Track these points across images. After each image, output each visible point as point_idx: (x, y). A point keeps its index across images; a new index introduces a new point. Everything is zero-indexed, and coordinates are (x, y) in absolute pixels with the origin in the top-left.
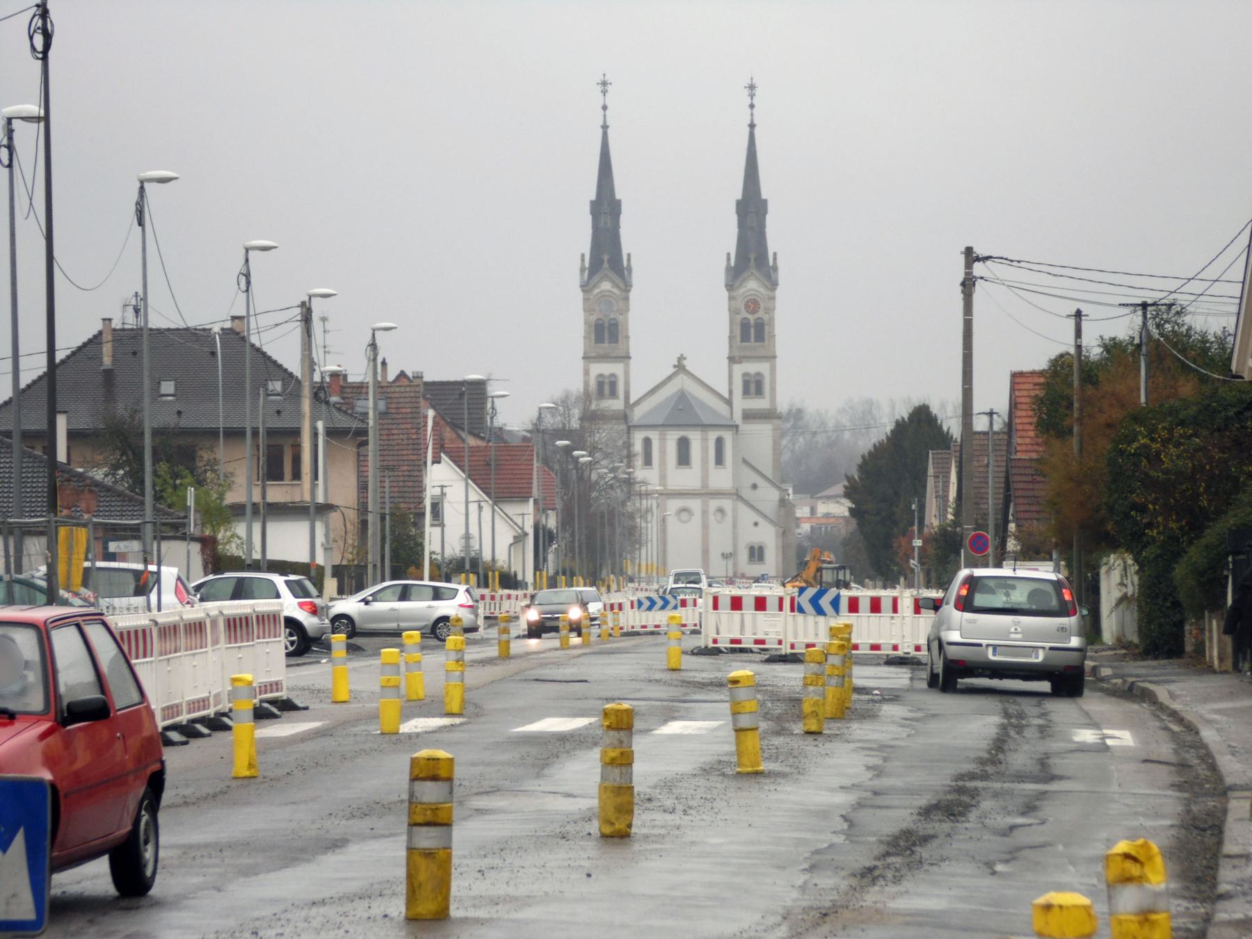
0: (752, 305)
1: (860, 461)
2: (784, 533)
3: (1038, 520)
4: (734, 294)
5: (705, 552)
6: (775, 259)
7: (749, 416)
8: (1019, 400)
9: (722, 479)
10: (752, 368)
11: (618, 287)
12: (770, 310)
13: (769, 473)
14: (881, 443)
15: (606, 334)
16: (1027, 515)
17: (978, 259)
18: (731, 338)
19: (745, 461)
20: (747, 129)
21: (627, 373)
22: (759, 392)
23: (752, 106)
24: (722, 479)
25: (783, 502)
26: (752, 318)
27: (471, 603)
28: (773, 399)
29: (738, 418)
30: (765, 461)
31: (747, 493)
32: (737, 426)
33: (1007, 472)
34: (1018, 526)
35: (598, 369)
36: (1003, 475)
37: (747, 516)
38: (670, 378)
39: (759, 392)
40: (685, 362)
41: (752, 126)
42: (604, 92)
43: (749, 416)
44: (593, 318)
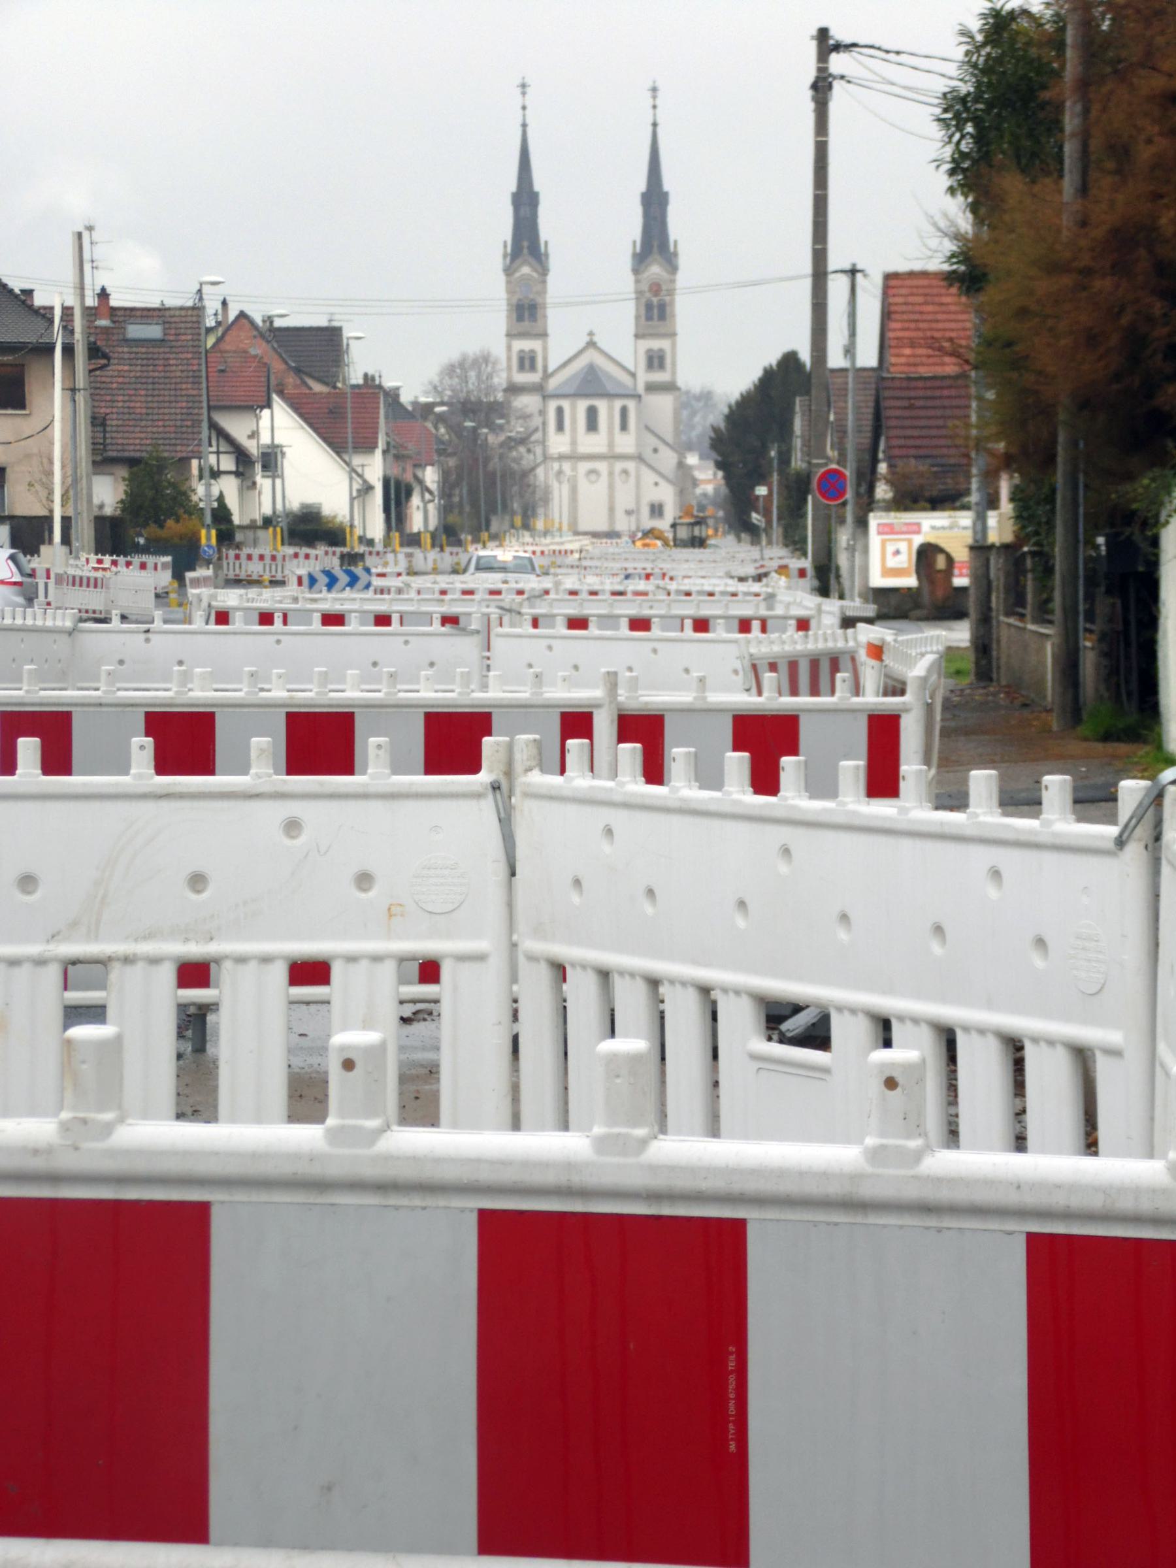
0: (656, 288)
1: (726, 410)
2: (681, 492)
3: (916, 457)
4: (640, 277)
5: (612, 510)
6: (675, 246)
7: (651, 388)
8: (893, 308)
9: (626, 443)
10: (655, 344)
11: (536, 271)
12: (671, 292)
13: (669, 438)
14: (749, 393)
15: (526, 313)
16: (904, 452)
17: (838, 47)
18: (637, 317)
19: (647, 428)
20: (650, 128)
21: (545, 349)
22: (662, 366)
23: (654, 107)
24: (626, 443)
25: (681, 465)
26: (655, 300)
27: (17, 578)
28: (674, 373)
29: (641, 389)
30: (666, 428)
31: (648, 454)
32: (639, 397)
33: (877, 390)
34: (890, 466)
35: (520, 345)
36: (872, 398)
37: (649, 477)
38: (581, 352)
39: (662, 366)
40: (596, 339)
41: (655, 125)
42: (524, 94)
43: (651, 388)
44: (514, 301)
